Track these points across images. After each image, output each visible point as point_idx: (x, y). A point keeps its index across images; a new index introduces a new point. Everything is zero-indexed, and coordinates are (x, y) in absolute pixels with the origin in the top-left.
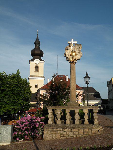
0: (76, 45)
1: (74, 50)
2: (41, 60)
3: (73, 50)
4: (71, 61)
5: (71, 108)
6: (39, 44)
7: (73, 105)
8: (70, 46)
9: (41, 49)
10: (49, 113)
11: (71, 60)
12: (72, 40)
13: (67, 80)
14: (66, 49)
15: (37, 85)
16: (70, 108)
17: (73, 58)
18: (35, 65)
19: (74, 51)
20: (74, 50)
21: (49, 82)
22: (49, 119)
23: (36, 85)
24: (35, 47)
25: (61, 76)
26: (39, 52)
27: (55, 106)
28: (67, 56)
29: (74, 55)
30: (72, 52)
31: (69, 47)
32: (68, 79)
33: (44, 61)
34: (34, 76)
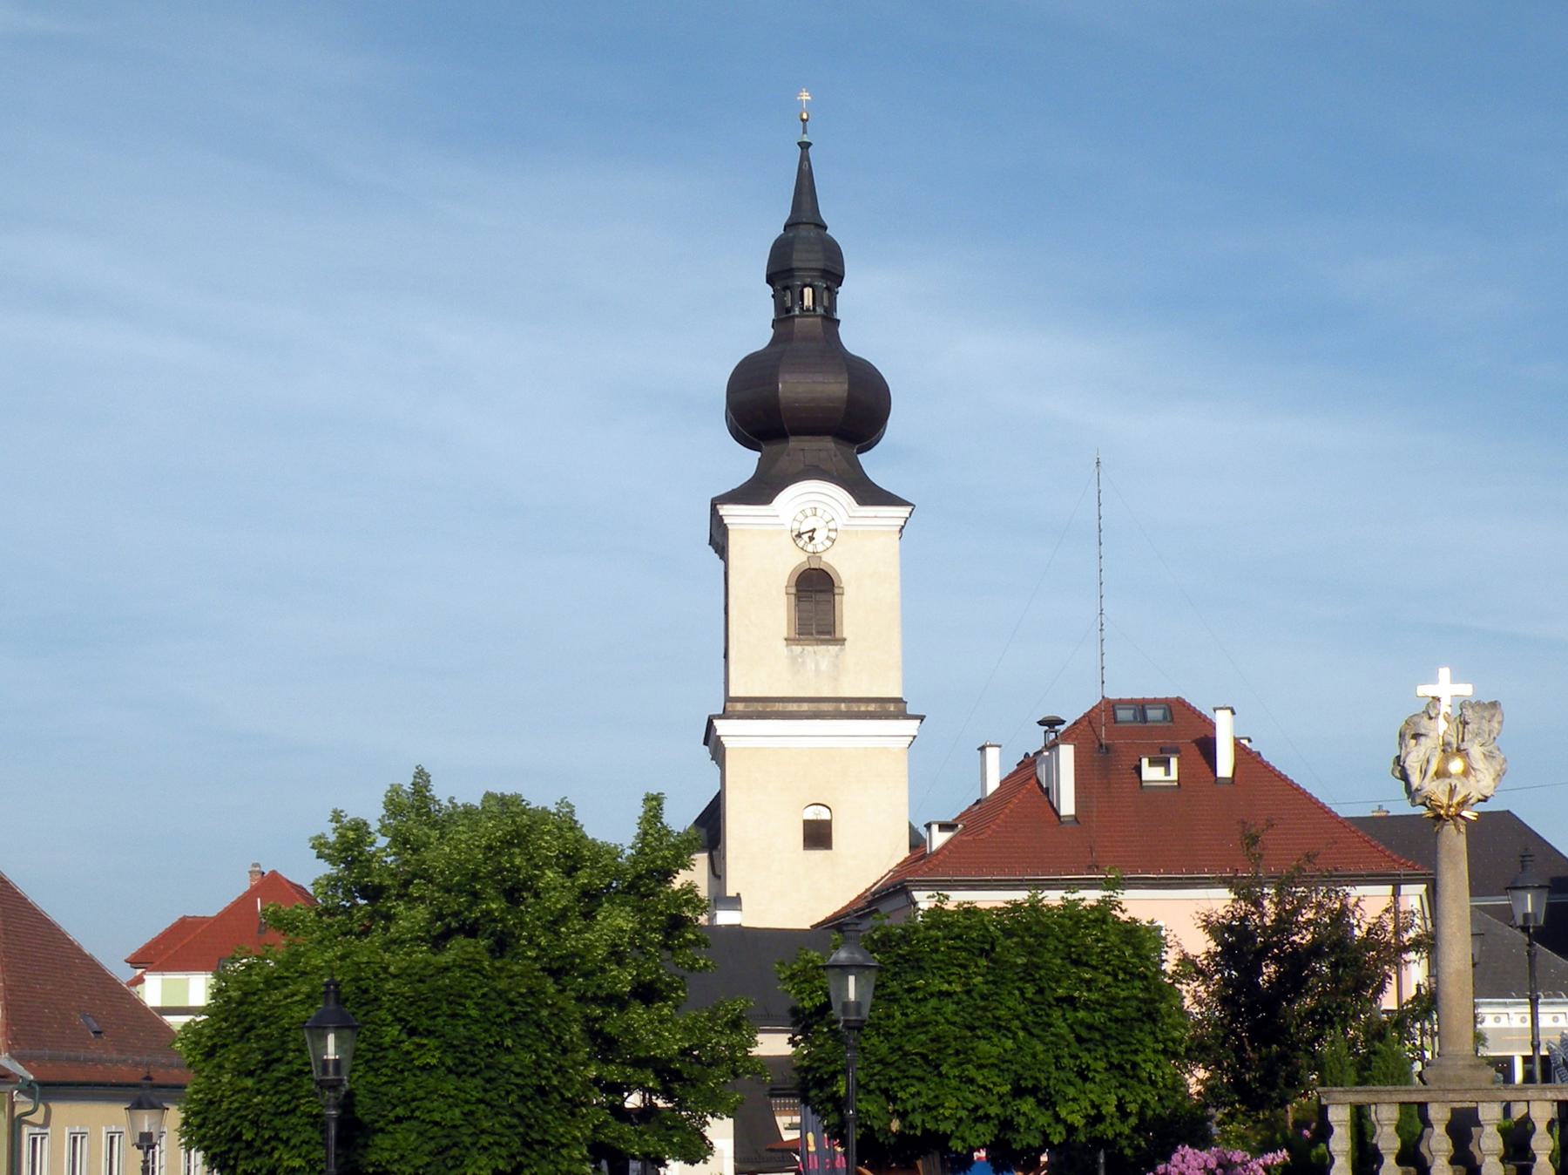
0: (1469, 714)
1: (1454, 741)
2: (868, 493)
3: (1449, 744)
4: (1442, 812)
5: (1456, 1097)
6: (833, 276)
7: (1461, 1080)
8: (1431, 718)
9: (855, 338)
10: (1337, 1130)
11: (1441, 807)
12: (1444, 673)
13: (1225, 767)
14: (1407, 737)
15: (824, 815)
16: (1451, 1096)
17: (1452, 791)
18: (793, 560)
19: (1458, 750)
20: (1454, 741)
21: (993, 785)
22: (1447, 1131)
23: (811, 814)
24: (784, 316)
25: (1141, 706)
26: (832, 388)
27: (1367, 1088)
28: (1415, 780)
29: (1457, 776)
30: (1449, 750)
31: (1426, 718)
32: (1237, 744)
33: (908, 504)
34: (779, 707)
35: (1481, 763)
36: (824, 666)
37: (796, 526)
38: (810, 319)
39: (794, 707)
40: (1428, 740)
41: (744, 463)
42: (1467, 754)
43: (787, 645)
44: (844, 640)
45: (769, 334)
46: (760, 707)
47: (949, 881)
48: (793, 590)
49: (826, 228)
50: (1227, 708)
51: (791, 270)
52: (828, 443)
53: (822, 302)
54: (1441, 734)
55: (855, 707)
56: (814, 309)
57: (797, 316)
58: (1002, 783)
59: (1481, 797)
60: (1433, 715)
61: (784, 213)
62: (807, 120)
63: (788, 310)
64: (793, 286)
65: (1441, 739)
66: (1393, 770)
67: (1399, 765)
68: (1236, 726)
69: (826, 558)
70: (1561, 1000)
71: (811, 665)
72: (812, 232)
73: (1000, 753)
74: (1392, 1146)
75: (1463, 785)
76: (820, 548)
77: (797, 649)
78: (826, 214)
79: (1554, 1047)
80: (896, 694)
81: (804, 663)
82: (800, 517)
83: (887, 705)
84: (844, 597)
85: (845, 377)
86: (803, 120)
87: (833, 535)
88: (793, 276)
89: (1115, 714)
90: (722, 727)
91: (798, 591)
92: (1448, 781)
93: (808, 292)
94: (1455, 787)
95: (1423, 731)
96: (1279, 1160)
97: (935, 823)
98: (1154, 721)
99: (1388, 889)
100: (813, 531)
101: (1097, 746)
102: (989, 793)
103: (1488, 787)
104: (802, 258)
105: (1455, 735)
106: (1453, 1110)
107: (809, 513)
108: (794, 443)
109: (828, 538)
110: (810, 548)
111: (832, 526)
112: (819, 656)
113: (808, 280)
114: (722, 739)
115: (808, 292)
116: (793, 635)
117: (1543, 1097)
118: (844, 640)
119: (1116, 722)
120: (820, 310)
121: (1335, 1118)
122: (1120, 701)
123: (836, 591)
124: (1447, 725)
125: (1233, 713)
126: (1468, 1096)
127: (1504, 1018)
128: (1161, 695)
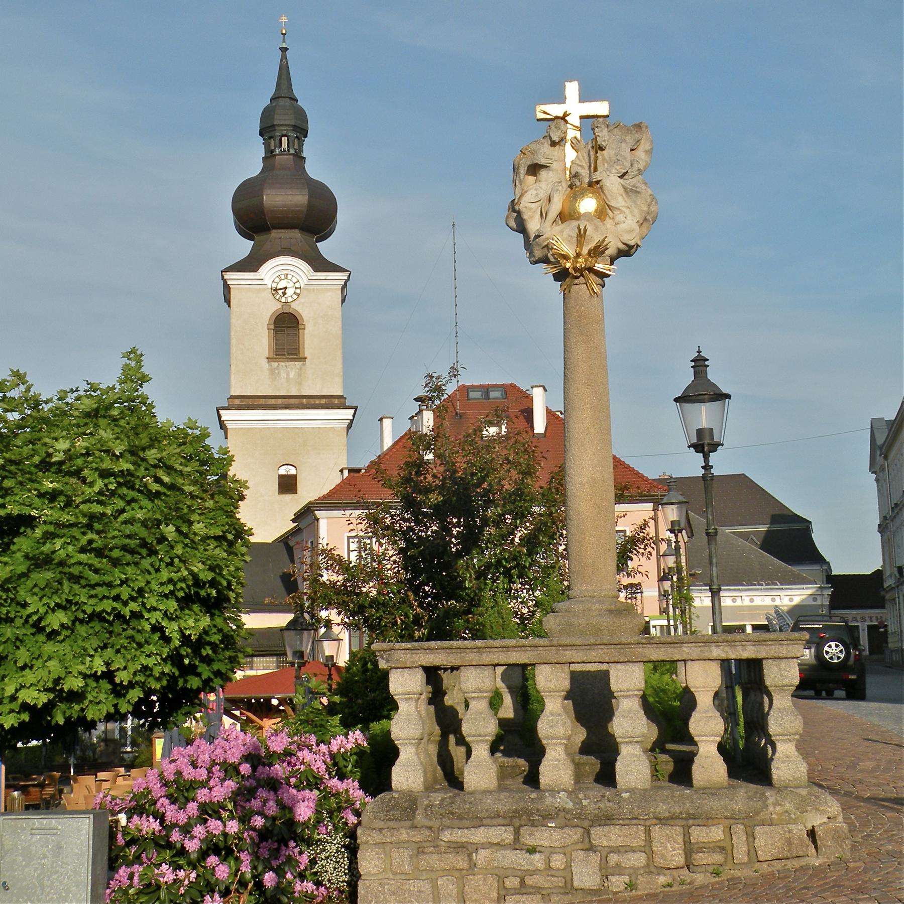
0: (603, 135)
1: (584, 173)
2: (320, 264)
4: (568, 265)
6: (301, 131)
7: (597, 631)
9: (314, 169)
10: (403, 706)
13: (540, 426)
15: (293, 471)
16: (569, 655)
17: (581, 236)
18: (272, 307)
19: (591, 184)
20: (584, 173)
21: (388, 442)
23: (283, 471)
24: (269, 155)
25: (486, 390)
28: (533, 226)
34: (263, 401)
35: (620, 199)
36: (292, 375)
37: (274, 285)
38: (286, 157)
39: (272, 402)
40: (551, 174)
41: (244, 247)
42: (601, 188)
43: (268, 362)
44: (306, 358)
45: (260, 166)
46: (250, 402)
47: (340, 503)
48: (272, 327)
49: (297, 101)
50: (540, 386)
51: (274, 126)
52: (296, 234)
53: (294, 146)
54: (568, 165)
55: (312, 401)
56: (288, 150)
57: (277, 155)
58: (395, 444)
59: (622, 246)
60: (556, 138)
61: (271, 91)
62: (285, 34)
63: (272, 151)
64: (275, 136)
65: (568, 173)
66: (507, 217)
67: (514, 211)
68: (547, 400)
69: (293, 306)
70: (777, 587)
71: (284, 375)
72: (288, 102)
73: (393, 423)
74: (482, 732)
75: (596, 228)
76: (290, 300)
77: (275, 364)
78: (297, 93)
79: (771, 617)
80: (339, 393)
81: (279, 373)
82: (277, 280)
83: (333, 400)
84: (306, 331)
85: (306, 191)
86: (282, 34)
87: (298, 291)
88: (275, 130)
89: (468, 394)
90: (226, 415)
91: (275, 327)
92: (575, 223)
93: (284, 139)
94: (585, 231)
95: (542, 161)
96: (349, 746)
97: (346, 469)
98: (494, 399)
99: (650, 506)
100: (286, 288)
101: (454, 414)
102: (385, 448)
103: (630, 231)
104: (283, 119)
105: (587, 168)
106: (574, 676)
107: (283, 277)
108: (275, 234)
109: (295, 293)
110: (283, 300)
111: (297, 285)
112: (290, 369)
113: (284, 133)
114: (225, 422)
115: (284, 139)
116: (272, 356)
117: (706, 655)
118: (306, 358)
119: (468, 399)
120: (292, 151)
121: (400, 690)
122: (473, 386)
123: (300, 327)
124: (575, 154)
125: (546, 390)
126: (593, 655)
127: (739, 599)
128: (500, 382)
